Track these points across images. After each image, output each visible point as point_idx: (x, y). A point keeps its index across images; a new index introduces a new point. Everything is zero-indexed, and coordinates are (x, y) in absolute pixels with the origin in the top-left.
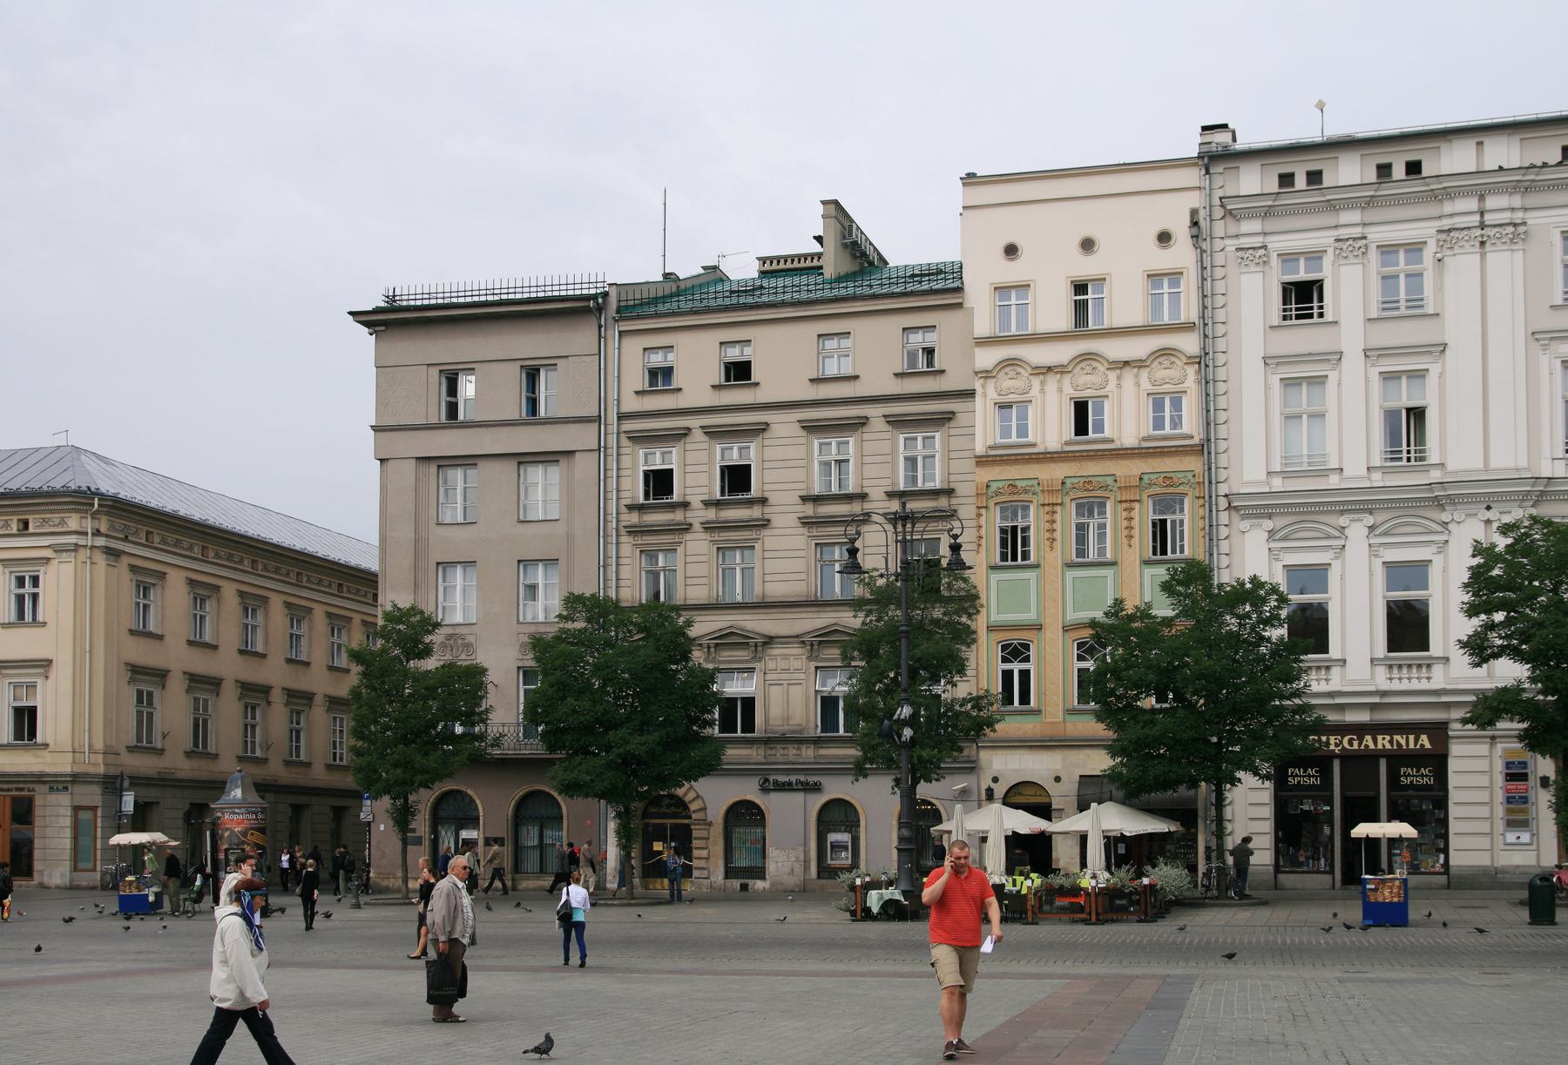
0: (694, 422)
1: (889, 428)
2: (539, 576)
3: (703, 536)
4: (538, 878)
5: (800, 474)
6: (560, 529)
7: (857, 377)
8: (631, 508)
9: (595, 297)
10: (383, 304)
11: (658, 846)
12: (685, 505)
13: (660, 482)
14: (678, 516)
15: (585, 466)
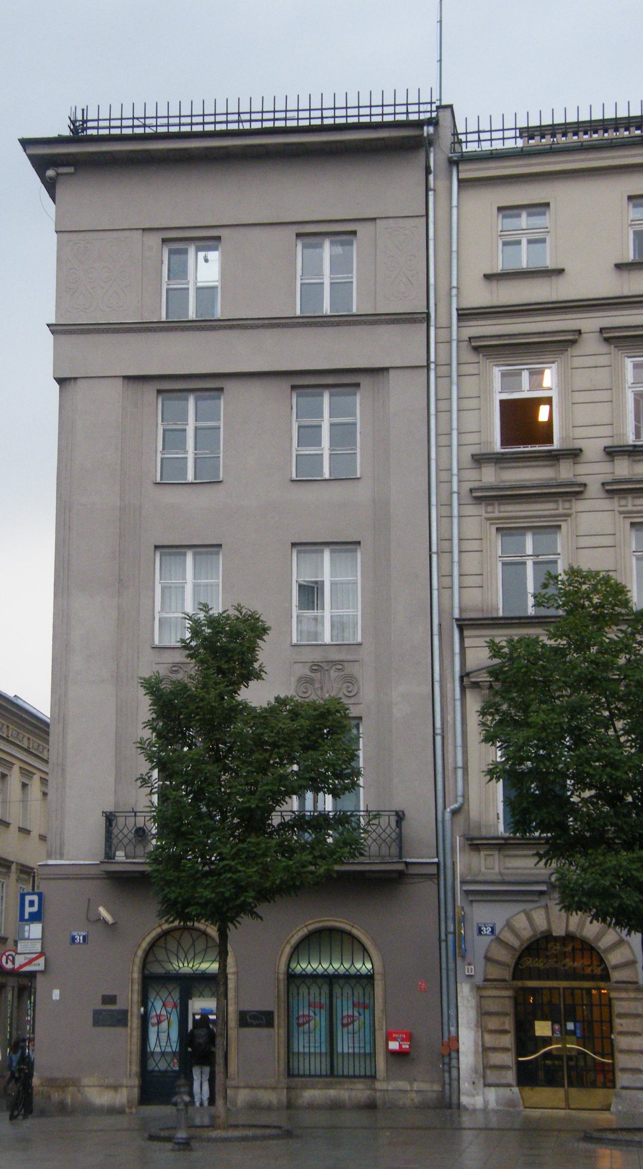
0: (590, 323)
1: (604, 348)
2: (326, 569)
3: (606, 504)
4: (329, 1086)
5: (602, 413)
6: (362, 493)
7: (561, 272)
8: (480, 460)
9: (419, 124)
10: (67, 133)
11: (543, 1028)
12: (574, 454)
13: (520, 421)
14: (565, 472)
15: (402, 392)
